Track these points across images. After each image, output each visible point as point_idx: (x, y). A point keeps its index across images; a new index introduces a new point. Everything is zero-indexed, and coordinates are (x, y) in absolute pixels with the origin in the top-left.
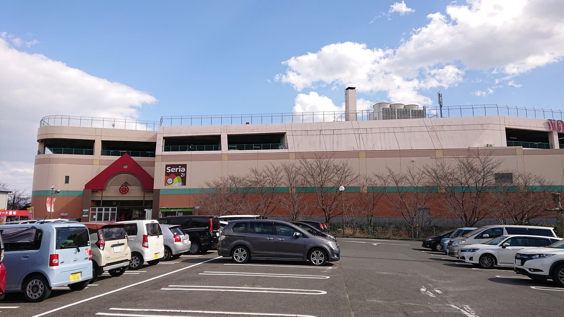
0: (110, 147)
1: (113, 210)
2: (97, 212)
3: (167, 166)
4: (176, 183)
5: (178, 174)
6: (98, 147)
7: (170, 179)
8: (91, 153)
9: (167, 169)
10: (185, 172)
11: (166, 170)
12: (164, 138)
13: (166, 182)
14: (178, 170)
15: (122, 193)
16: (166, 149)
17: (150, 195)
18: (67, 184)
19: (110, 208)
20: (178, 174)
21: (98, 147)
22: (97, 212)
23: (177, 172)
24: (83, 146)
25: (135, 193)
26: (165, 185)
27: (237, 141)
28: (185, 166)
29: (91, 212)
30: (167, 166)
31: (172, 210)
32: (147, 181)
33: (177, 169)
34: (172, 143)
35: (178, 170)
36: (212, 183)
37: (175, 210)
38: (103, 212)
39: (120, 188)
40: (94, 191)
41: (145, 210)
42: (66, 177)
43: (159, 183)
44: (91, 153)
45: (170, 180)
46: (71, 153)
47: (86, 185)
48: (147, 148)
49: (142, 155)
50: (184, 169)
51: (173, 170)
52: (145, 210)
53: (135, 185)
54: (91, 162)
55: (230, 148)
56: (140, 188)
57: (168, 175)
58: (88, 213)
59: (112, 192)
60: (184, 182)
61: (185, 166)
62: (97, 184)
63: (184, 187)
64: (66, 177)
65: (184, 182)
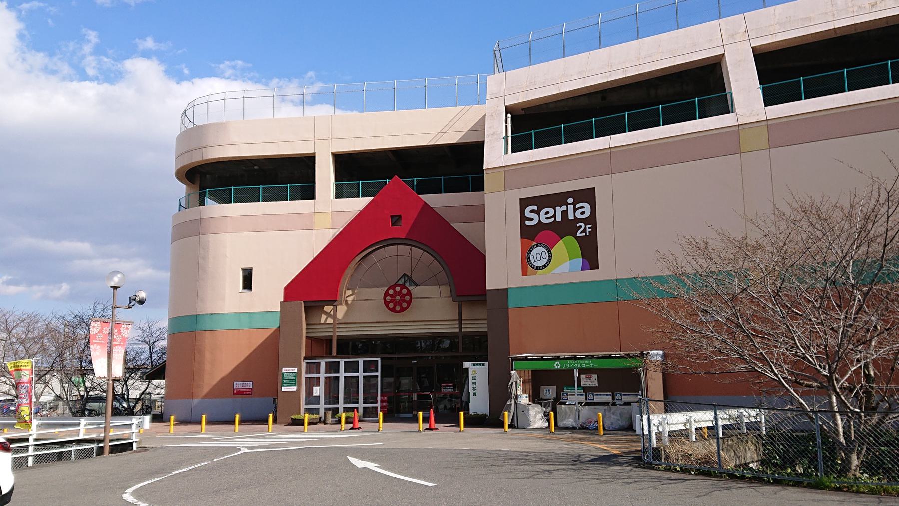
0: (354, 169)
1: (368, 367)
2: (323, 375)
3: (524, 203)
4: (563, 264)
5: (565, 228)
6: (325, 175)
7: (540, 249)
8: (308, 193)
9: (528, 214)
10: (592, 220)
11: (523, 218)
12: (508, 110)
13: (527, 265)
14: (565, 214)
15: (393, 310)
16: (519, 145)
17: (481, 312)
18: (247, 294)
19: (361, 361)
20: (565, 228)
21: (325, 175)
22: (323, 375)
23: (567, 221)
24: (286, 176)
25: (433, 312)
26: (525, 273)
27: (789, 69)
28: (588, 195)
29: (304, 375)
30: (524, 203)
31: (557, 365)
32: (463, 265)
33: (559, 210)
34: (535, 123)
35: (565, 214)
36: (715, 244)
37: (568, 365)
38: (342, 374)
39: (386, 294)
40: (313, 308)
41: (467, 365)
42: (244, 270)
43: (502, 270)
44: (308, 193)
45: (538, 254)
46: (254, 198)
47: (286, 289)
48: (460, 164)
49: (451, 188)
50: (587, 208)
51: (545, 216)
52: (467, 365)
53: (432, 280)
54: (309, 223)
55: (770, 99)
56: (445, 290)
57: (531, 235)
58: (295, 380)
59: (356, 310)
60: (591, 260)
61: (588, 195)
62: (312, 288)
63: (591, 275)
64: (244, 270)
65: (591, 260)
